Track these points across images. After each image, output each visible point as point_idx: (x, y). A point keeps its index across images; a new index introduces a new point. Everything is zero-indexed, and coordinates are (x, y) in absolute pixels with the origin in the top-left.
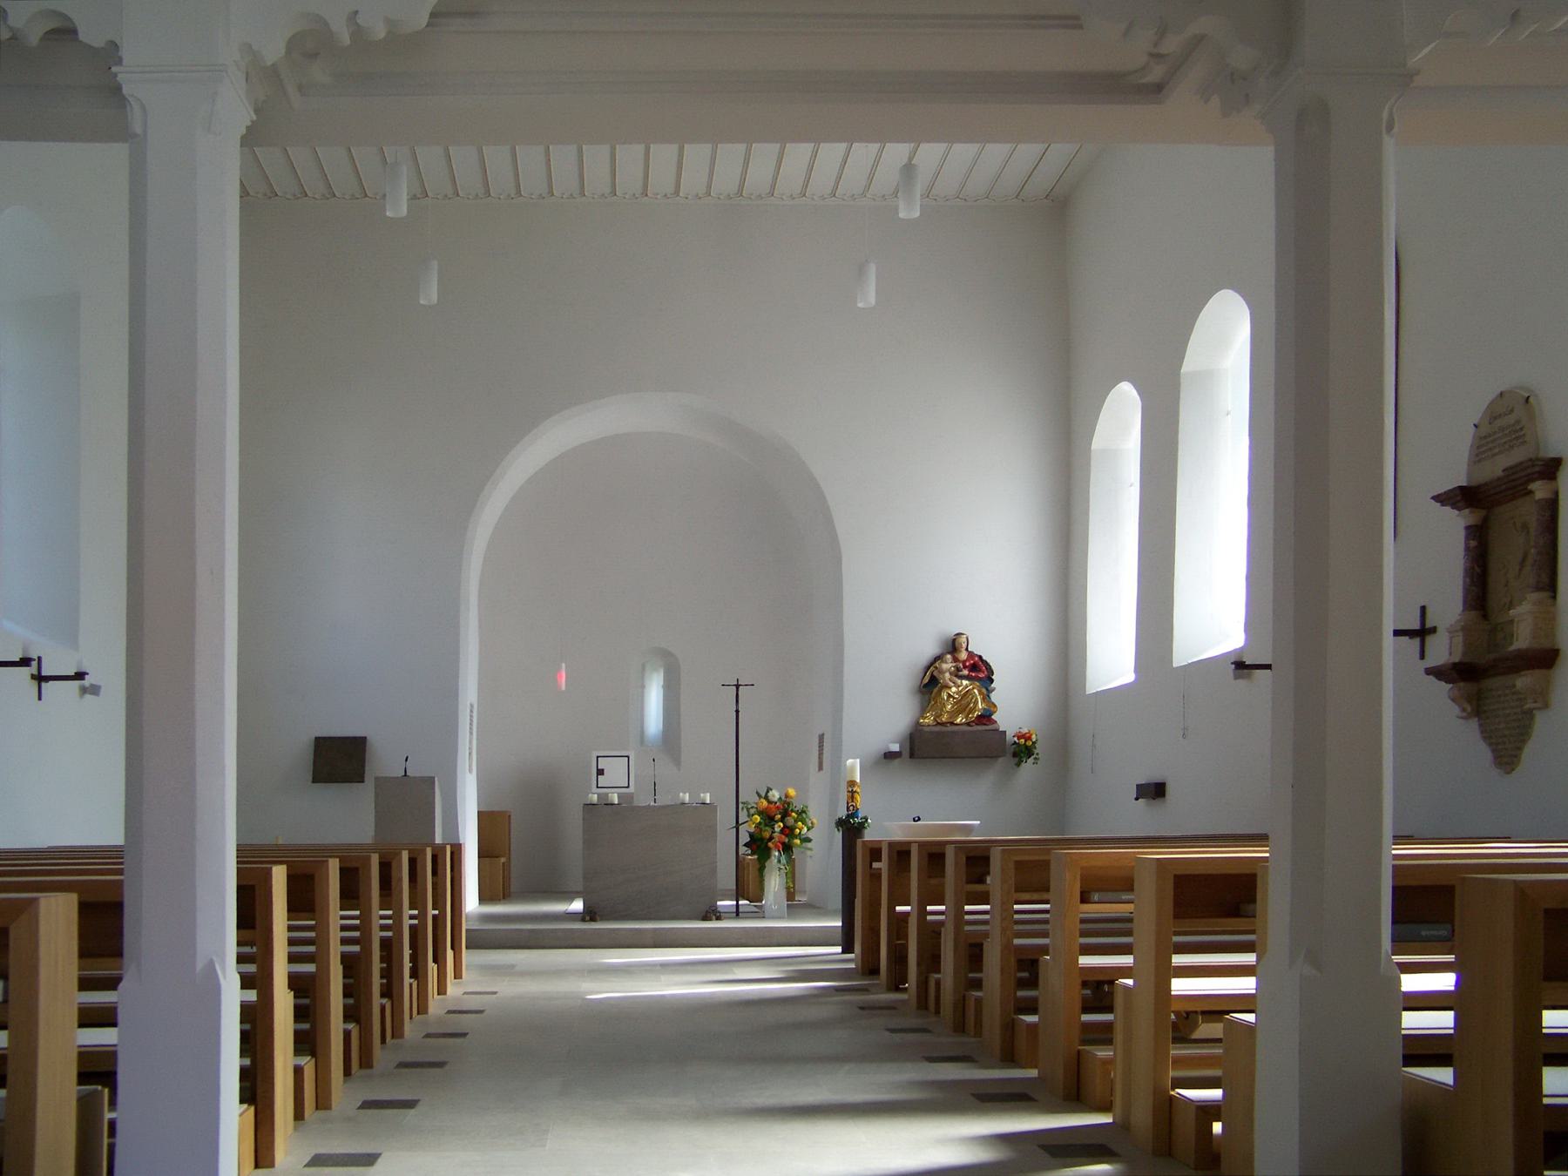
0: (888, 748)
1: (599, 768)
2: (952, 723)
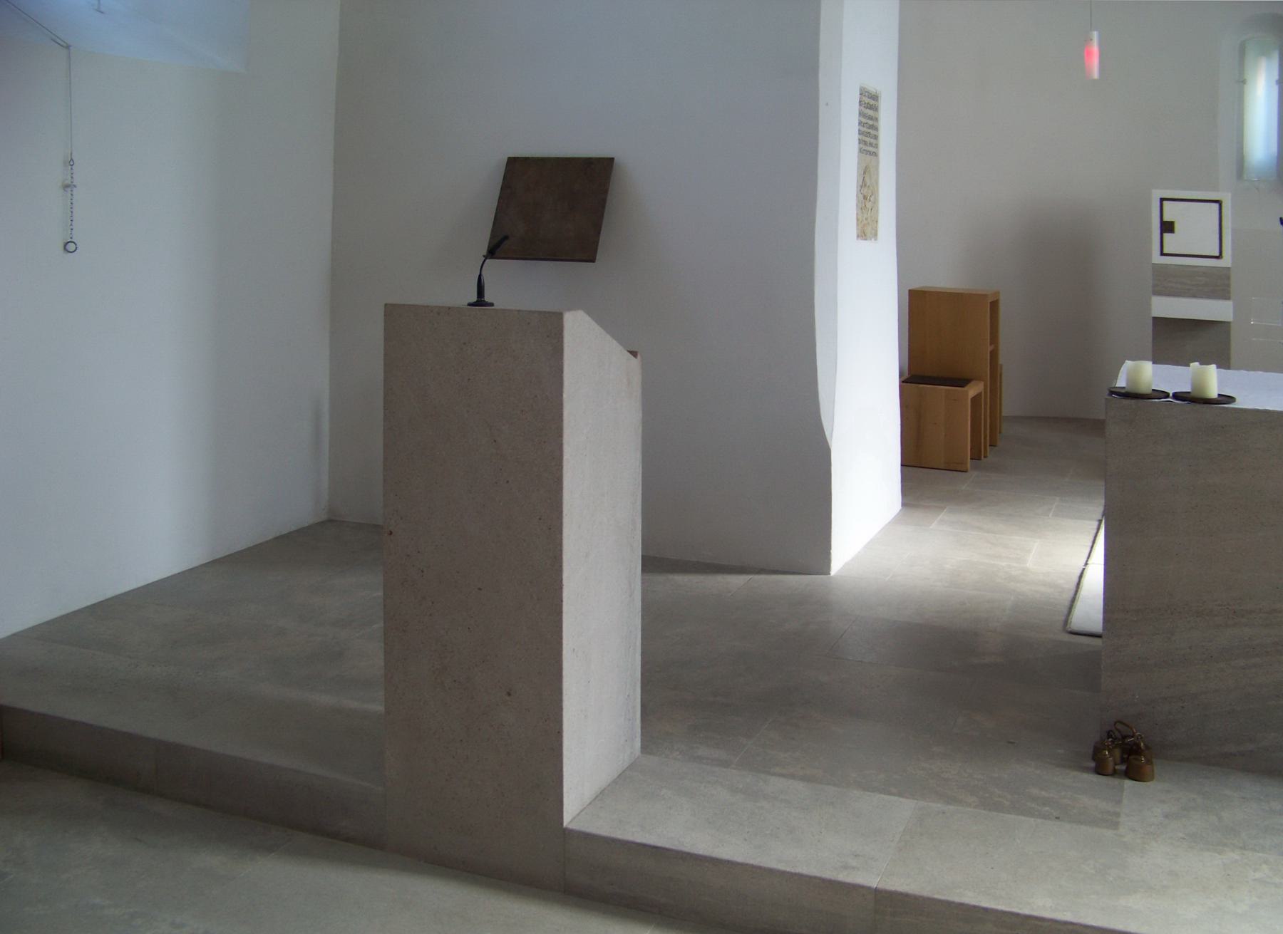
1: (1166, 218)
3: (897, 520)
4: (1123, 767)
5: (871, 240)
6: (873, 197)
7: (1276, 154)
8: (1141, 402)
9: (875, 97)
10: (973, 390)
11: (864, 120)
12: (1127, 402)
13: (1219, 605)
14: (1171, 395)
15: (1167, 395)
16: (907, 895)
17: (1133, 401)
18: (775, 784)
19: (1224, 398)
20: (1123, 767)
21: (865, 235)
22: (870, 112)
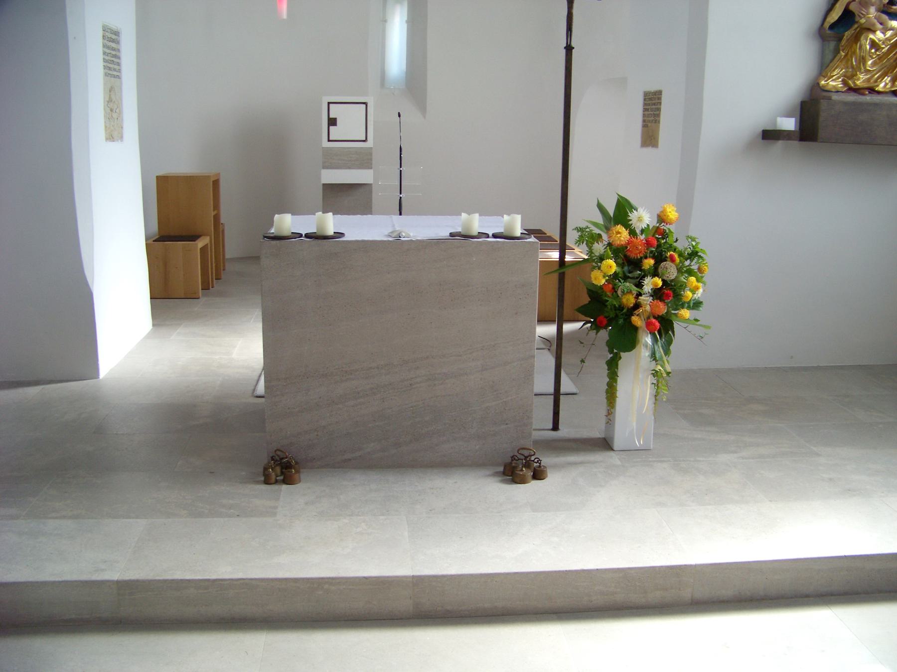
0: (775, 123)
1: (331, 116)
2: (872, 90)
3: (148, 336)
4: (282, 478)
5: (118, 141)
6: (118, 109)
7: (405, 70)
8: (283, 242)
9: (117, 33)
10: (200, 243)
11: (108, 51)
12: (274, 242)
13: (336, 369)
14: (304, 235)
15: (301, 235)
16: (138, 581)
17: (278, 242)
18: (51, 524)
19: (293, 235)
20: (282, 478)
21: (113, 138)
22: (113, 45)
